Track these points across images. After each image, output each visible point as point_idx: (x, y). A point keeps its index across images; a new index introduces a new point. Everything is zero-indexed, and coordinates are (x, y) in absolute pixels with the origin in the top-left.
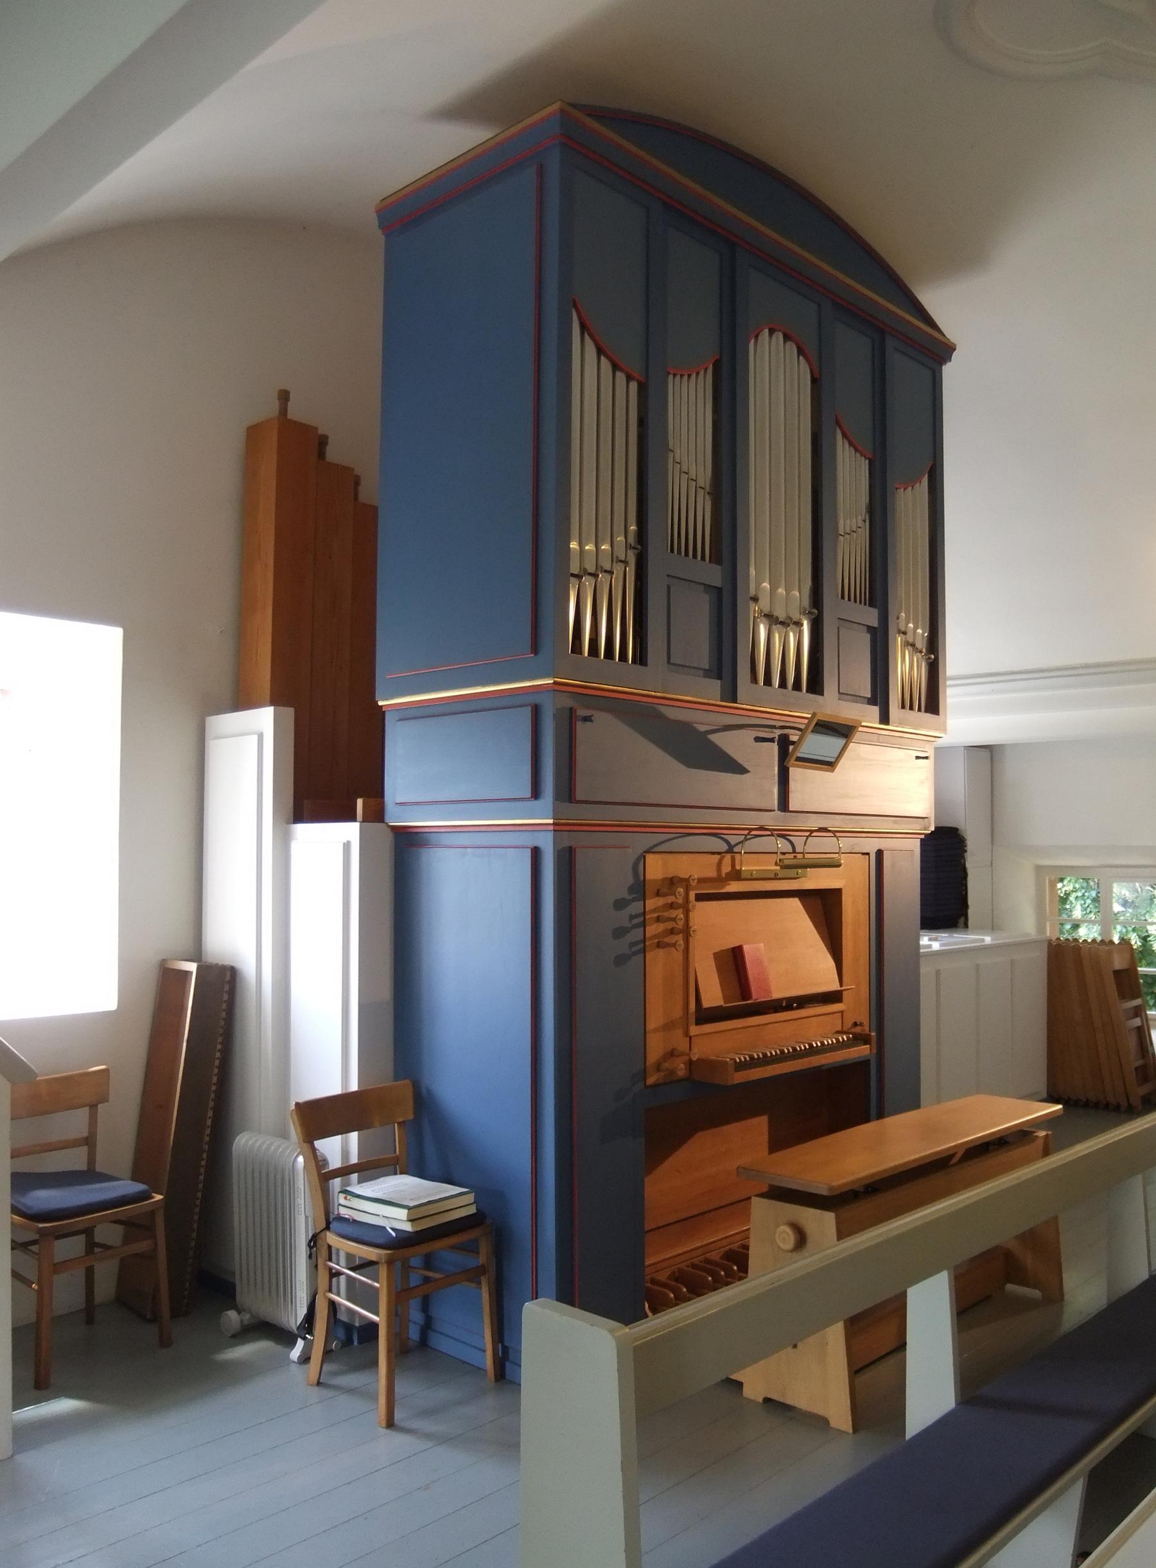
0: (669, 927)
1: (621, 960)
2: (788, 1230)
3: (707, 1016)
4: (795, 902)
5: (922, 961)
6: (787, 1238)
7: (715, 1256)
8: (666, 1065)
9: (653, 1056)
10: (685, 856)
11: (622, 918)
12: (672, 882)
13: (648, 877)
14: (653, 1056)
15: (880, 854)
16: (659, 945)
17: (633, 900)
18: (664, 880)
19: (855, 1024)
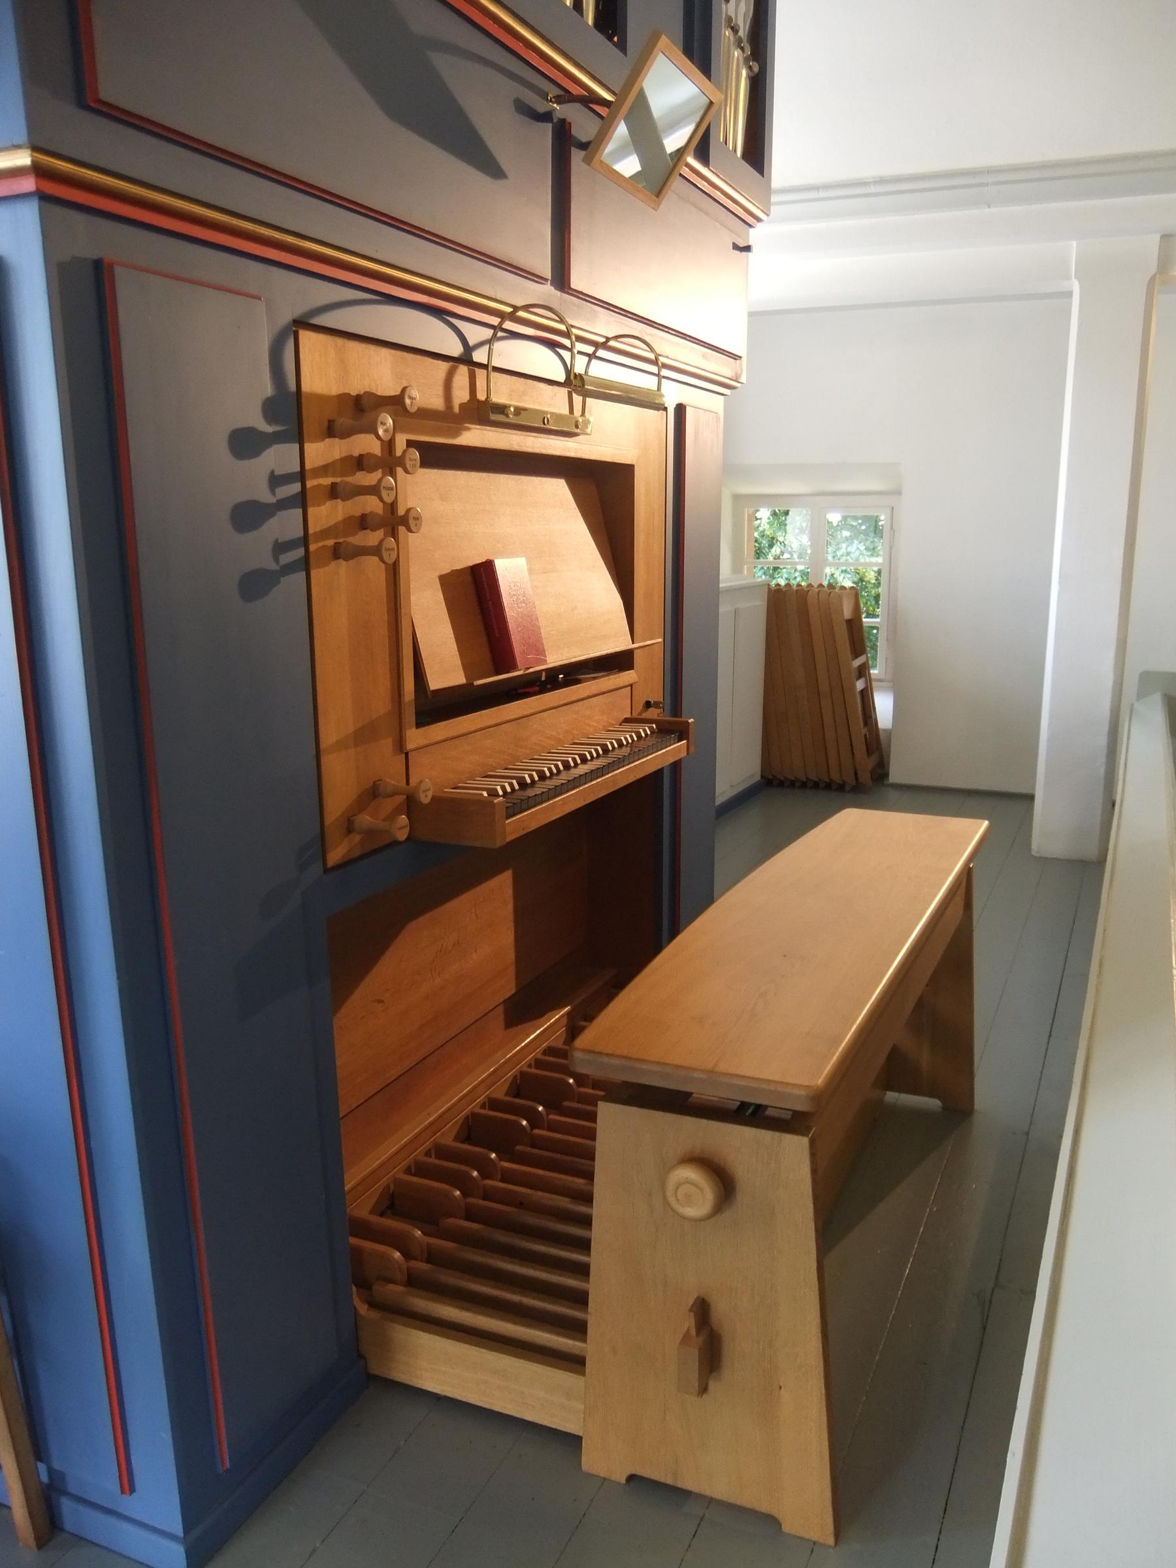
0: (358, 512)
1: (255, 585)
2: (690, 1173)
3: (439, 707)
4: (557, 489)
5: (722, 598)
6: (692, 1191)
7: (447, 1137)
8: (365, 820)
9: (337, 803)
10: (384, 352)
11: (253, 478)
12: (360, 409)
13: (306, 387)
14: (337, 803)
15: (680, 410)
16: (337, 553)
17: (277, 438)
18: (343, 398)
19: (648, 705)
